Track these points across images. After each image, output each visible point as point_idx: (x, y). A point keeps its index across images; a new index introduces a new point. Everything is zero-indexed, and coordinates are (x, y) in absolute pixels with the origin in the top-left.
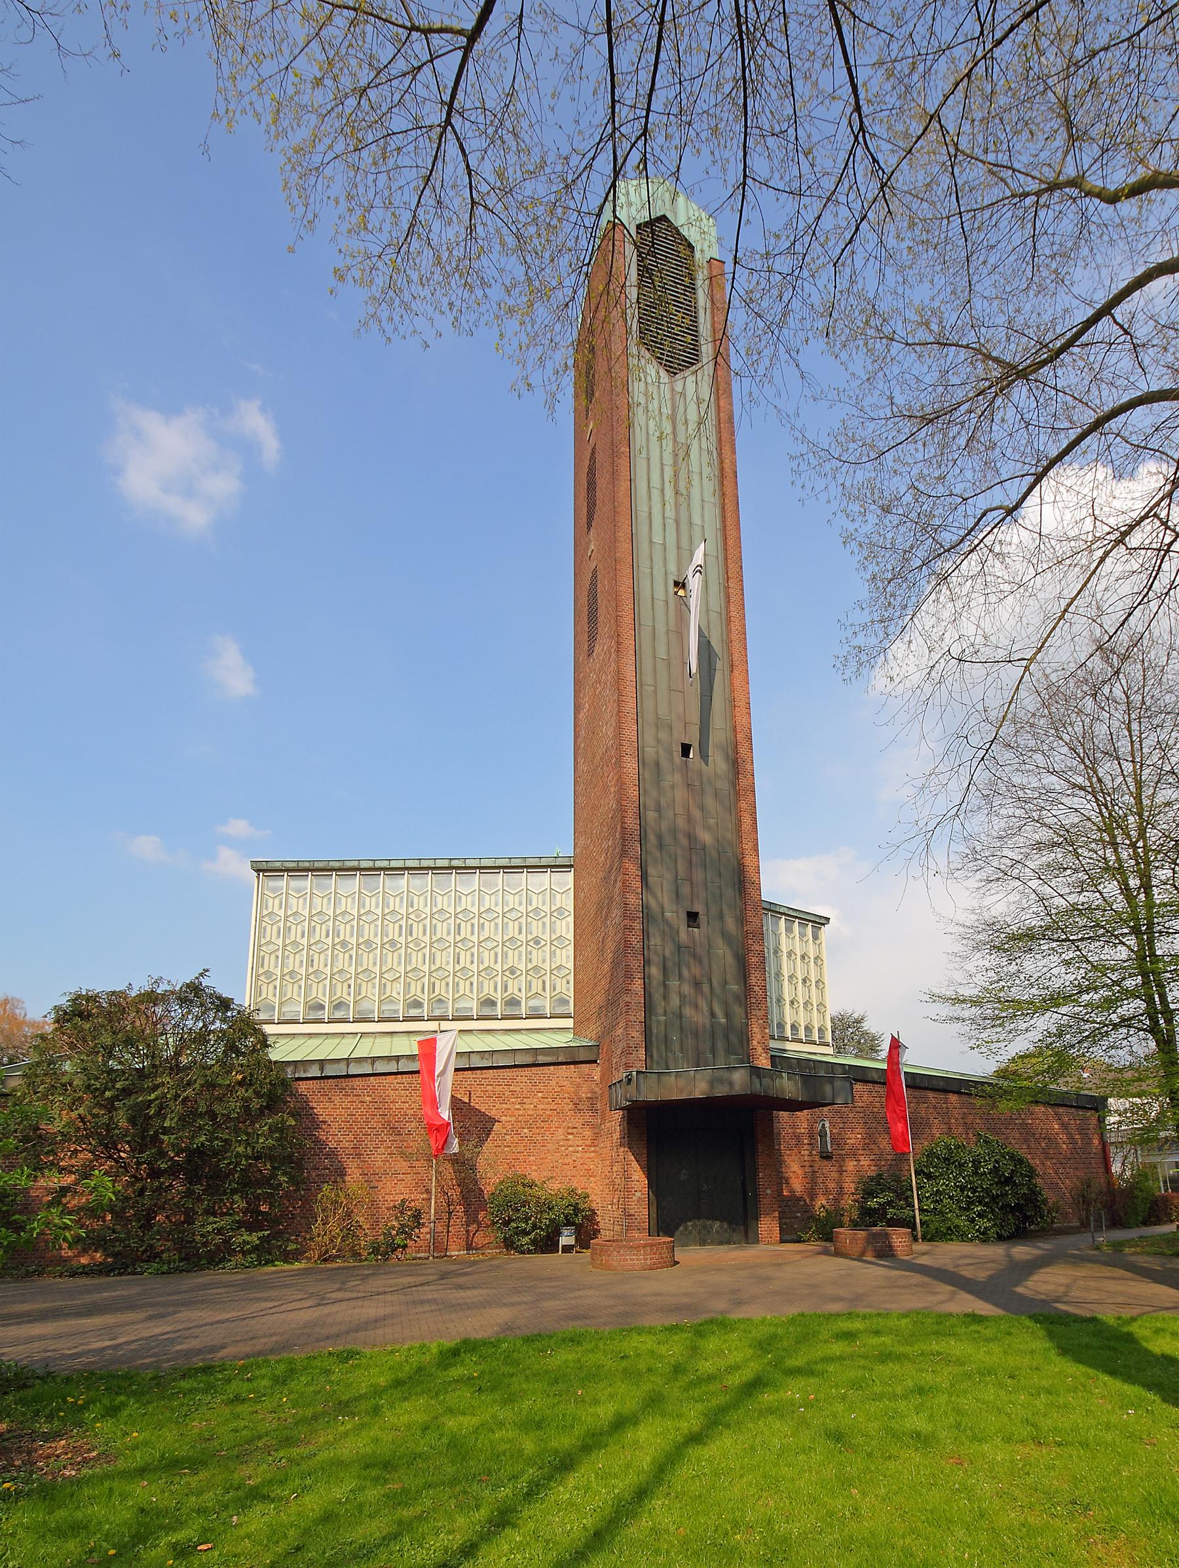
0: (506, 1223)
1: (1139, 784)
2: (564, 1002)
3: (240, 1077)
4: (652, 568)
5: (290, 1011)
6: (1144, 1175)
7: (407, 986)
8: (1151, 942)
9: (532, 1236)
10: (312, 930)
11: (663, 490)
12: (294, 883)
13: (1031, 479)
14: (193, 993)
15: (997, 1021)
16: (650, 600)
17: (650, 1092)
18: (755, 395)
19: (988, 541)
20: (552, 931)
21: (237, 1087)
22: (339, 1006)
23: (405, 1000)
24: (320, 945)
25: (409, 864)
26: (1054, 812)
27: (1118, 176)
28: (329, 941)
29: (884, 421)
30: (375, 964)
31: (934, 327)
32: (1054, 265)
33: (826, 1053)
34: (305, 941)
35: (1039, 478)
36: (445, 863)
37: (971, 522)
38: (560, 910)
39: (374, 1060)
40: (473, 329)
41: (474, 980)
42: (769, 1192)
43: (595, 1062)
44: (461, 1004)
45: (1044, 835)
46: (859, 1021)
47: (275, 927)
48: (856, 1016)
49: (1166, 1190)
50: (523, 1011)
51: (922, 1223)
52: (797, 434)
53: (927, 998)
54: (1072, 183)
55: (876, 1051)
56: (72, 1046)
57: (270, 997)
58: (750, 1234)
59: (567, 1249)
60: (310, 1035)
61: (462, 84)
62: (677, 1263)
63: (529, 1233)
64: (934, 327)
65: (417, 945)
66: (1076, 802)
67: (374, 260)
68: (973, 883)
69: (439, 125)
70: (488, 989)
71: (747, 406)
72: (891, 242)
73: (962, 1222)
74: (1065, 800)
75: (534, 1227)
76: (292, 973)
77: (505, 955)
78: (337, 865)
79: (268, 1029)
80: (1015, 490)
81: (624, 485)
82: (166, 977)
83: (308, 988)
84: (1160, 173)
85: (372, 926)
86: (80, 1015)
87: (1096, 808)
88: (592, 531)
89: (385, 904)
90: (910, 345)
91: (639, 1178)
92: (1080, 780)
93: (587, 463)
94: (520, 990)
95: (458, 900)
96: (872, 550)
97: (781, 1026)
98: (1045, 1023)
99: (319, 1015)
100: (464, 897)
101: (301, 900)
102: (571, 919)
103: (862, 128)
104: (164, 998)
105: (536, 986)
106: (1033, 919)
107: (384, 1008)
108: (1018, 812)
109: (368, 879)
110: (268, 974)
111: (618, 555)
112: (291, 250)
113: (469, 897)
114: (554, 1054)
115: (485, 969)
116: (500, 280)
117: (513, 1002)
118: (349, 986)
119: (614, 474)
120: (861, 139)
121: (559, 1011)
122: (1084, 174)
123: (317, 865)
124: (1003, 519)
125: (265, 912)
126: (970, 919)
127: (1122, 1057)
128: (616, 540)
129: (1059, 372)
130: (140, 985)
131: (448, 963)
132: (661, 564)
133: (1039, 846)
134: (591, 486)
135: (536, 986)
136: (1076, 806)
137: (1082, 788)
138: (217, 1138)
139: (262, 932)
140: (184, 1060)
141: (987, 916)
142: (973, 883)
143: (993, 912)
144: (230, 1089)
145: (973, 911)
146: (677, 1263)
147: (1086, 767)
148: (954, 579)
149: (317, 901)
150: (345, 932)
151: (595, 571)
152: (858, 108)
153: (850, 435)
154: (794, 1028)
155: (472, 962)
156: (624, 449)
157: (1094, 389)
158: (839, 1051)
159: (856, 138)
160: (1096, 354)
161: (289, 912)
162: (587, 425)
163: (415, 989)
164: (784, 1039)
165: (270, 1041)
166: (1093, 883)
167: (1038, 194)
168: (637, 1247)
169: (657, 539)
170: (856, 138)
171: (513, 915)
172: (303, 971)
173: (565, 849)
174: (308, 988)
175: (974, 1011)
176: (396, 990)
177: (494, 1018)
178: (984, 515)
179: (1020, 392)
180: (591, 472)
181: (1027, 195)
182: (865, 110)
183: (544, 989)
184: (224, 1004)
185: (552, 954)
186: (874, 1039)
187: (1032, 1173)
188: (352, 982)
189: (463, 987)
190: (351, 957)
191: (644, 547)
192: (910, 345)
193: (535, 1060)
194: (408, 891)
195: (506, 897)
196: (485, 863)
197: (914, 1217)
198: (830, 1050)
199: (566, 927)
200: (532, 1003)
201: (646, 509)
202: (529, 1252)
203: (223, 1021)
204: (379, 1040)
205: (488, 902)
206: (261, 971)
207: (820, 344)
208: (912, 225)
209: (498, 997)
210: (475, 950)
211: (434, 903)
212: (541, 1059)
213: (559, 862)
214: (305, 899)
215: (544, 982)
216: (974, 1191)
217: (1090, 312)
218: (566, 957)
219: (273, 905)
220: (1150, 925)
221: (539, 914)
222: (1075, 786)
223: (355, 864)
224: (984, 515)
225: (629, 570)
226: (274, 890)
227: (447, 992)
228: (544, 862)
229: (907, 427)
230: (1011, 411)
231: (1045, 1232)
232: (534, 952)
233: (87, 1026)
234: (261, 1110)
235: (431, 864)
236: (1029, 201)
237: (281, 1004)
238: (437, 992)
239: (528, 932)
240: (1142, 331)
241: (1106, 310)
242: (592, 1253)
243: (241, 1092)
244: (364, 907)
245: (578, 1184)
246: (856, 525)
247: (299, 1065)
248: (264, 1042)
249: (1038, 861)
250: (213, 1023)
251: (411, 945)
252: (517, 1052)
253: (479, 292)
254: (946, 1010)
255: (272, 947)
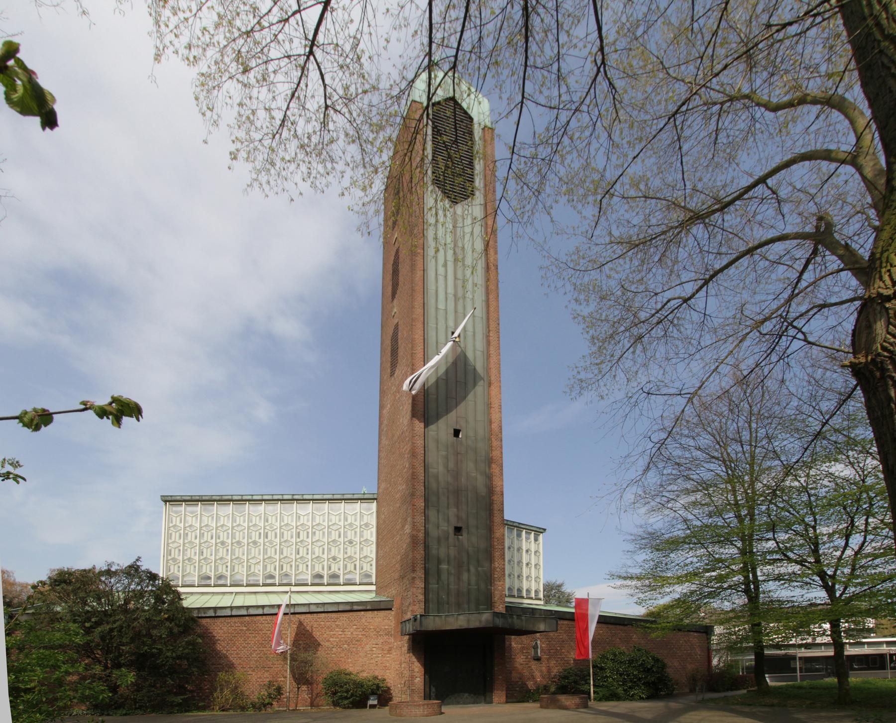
0: (335, 693)
1: (753, 457)
2: (369, 576)
3: (166, 616)
4: (437, 324)
5: (188, 580)
6: (730, 666)
7: (265, 567)
8: (751, 545)
9: (351, 700)
10: (202, 535)
11: (446, 277)
12: (189, 509)
13: (700, 283)
14: (133, 571)
15: (651, 588)
16: (435, 344)
17: (435, 623)
18: (520, 233)
19: (670, 317)
20: (361, 536)
21: (165, 621)
22: (220, 577)
23: (263, 575)
24: (207, 544)
25: (265, 497)
26: (698, 472)
27: (778, 95)
28: (213, 541)
29: (604, 246)
30: (243, 554)
31: (642, 187)
32: (728, 151)
33: (539, 604)
34: (197, 541)
35: (706, 282)
36: (290, 497)
37: (659, 306)
38: (367, 525)
39: (248, 607)
40: (325, 189)
41: (309, 564)
42: (500, 677)
43: (391, 609)
44: (301, 577)
45: (689, 485)
46: (560, 586)
47: (178, 534)
48: (558, 583)
49: (743, 673)
50: (341, 581)
51: (594, 692)
52: (545, 253)
53: (608, 577)
54: (747, 97)
55: (570, 603)
56: (60, 598)
57: (176, 572)
58: (488, 699)
59: (373, 707)
60: (203, 593)
61: (322, 29)
62: (443, 713)
63: (349, 698)
64: (642, 187)
65: (271, 543)
66: (712, 466)
67: (256, 143)
68: (643, 510)
69: (304, 55)
70: (318, 569)
71: (515, 239)
72: (616, 137)
73: (620, 691)
74: (705, 465)
75: (352, 695)
76: (189, 559)
77: (329, 550)
78: (218, 498)
79: (181, 590)
80: (689, 289)
81: (419, 273)
82: (116, 561)
83: (200, 567)
84: (808, 95)
85: (241, 533)
86: (65, 582)
87: (724, 469)
88: (395, 301)
89: (250, 520)
90: (625, 198)
91: (418, 668)
92: (716, 454)
93: (392, 258)
94: (339, 569)
95: (298, 517)
96: (591, 322)
97: (519, 590)
98: (679, 590)
99: (208, 582)
100: (302, 517)
101: (194, 518)
102: (374, 530)
103: (603, 62)
104: (115, 573)
105: (350, 567)
106: (679, 532)
107: (249, 578)
108: (674, 472)
109: (238, 506)
110: (174, 560)
111: (414, 316)
112: (205, 142)
113: (306, 517)
114: (363, 605)
115: (316, 558)
116: (343, 157)
117: (335, 576)
118: (227, 567)
119: (413, 267)
120: (602, 69)
121: (365, 581)
122: (756, 91)
123: (204, 498)
124: (681, 305)
125: (171, 525)
126: (640, 531)
127: (727, 606)
128: (413, 307)
129: (727, 217)
130: (101, 566)
131: (291, 554)
132: (443, 322)
133: (687, 492)
134: (395, 272)
135: (350, 567)
136: (712, 468)
137: (717, 458)
138: (154, 648)
139: (169, 536)
140: (131, 606)
141: (650, 530)
142: (643, 510)
143: (654, 527)
144: (161, 622)
145: (641, 526)
146: (443, 713)
147: (720, 446)
148: (646, 339)
149: (205, 519)
150: (223, 536)
151: (397, 326)
152: (602, 49)
153: (581, 254)
154: (528, 591)
155: (308, 554)
156: (420, 251)
157: (747, 229)
158: (547, 602)
159: (599, 69)
160: (753, 206)
161: (187, 525)
162: (393, 235)
163: (270, 569)
164: (522, 597)
165: (183, 597)
166: (719, 512)
167: (722, 104)
168: (419, 706)
169: (441, 306)
170: (599, 69)
171: (335, 527)
172: (197, 558)
173: (370, 487)
174: (200, 567)
175: (639, 584)
176: (258, 570)
177: (322, 585)
178: (669, 301)
179: (698, 230)
180: (396, 264)
181: (715, 104)
182: (606, 49)
183: (355, 569)
184: (153, 577)
185: (361, 549)
186: (569, 595)
187: (664, 666)
188: (229, 564)
189: (302, 568)
190: (228, 550)
191: (431, 311)
192: (625, 198)
193: (352, 608)
194: (265, 513)
195: (330, 517)
196: (316, 497)
197: (590, 689)
198: (542, 602)
199: (371, 534)
200: (347, 577)
201: (434, 288)
202: (348, 708)
203: (153, 586)
204: (247, 596)
205: (318, 520)
206: (169, 558)
207: (563, 199)
208: (631, 127)
209: (325, 573)
210: (310, 547)
211: (282, 520)
212: (355, 608)
213: (366, 496)
214: (197, 518)
215: (355, 565)
216: (628, 675)
217: (751, 181)
218: (371, 551)
219: (176, 521)
220: (751, 536)
221: (352, 527)
222: (713, 457)
223: (230, 497)
224: (669, 301)
225: (422, 326)
226: (176, 512)
227: (291, 570)
228: (356, 496)
229: (619, 250)
230: (691, 240)
231: (670, 696)
232: (349, 548)
233: (70, 588)
234: (181, 633)
235: (280, 497)
236: (716, 108)
237: (183, 576)
238: (284, 570)
239: (345, 536)
240: (783, 193)
241: (762, 180)
242: (390, 709)
243: (167, 624)
244: (235, 522)
245: (379, 673)
246: (582, 307)
247: (201, 610)
248: (178, 596)
249: (684, 500)
250: (147, 586)
251: (267, 544)
252: (296, 606)
253: (329, 165)
254: (619, 582)
255: (175, 545)
